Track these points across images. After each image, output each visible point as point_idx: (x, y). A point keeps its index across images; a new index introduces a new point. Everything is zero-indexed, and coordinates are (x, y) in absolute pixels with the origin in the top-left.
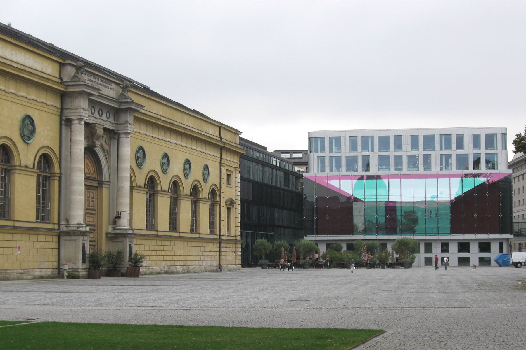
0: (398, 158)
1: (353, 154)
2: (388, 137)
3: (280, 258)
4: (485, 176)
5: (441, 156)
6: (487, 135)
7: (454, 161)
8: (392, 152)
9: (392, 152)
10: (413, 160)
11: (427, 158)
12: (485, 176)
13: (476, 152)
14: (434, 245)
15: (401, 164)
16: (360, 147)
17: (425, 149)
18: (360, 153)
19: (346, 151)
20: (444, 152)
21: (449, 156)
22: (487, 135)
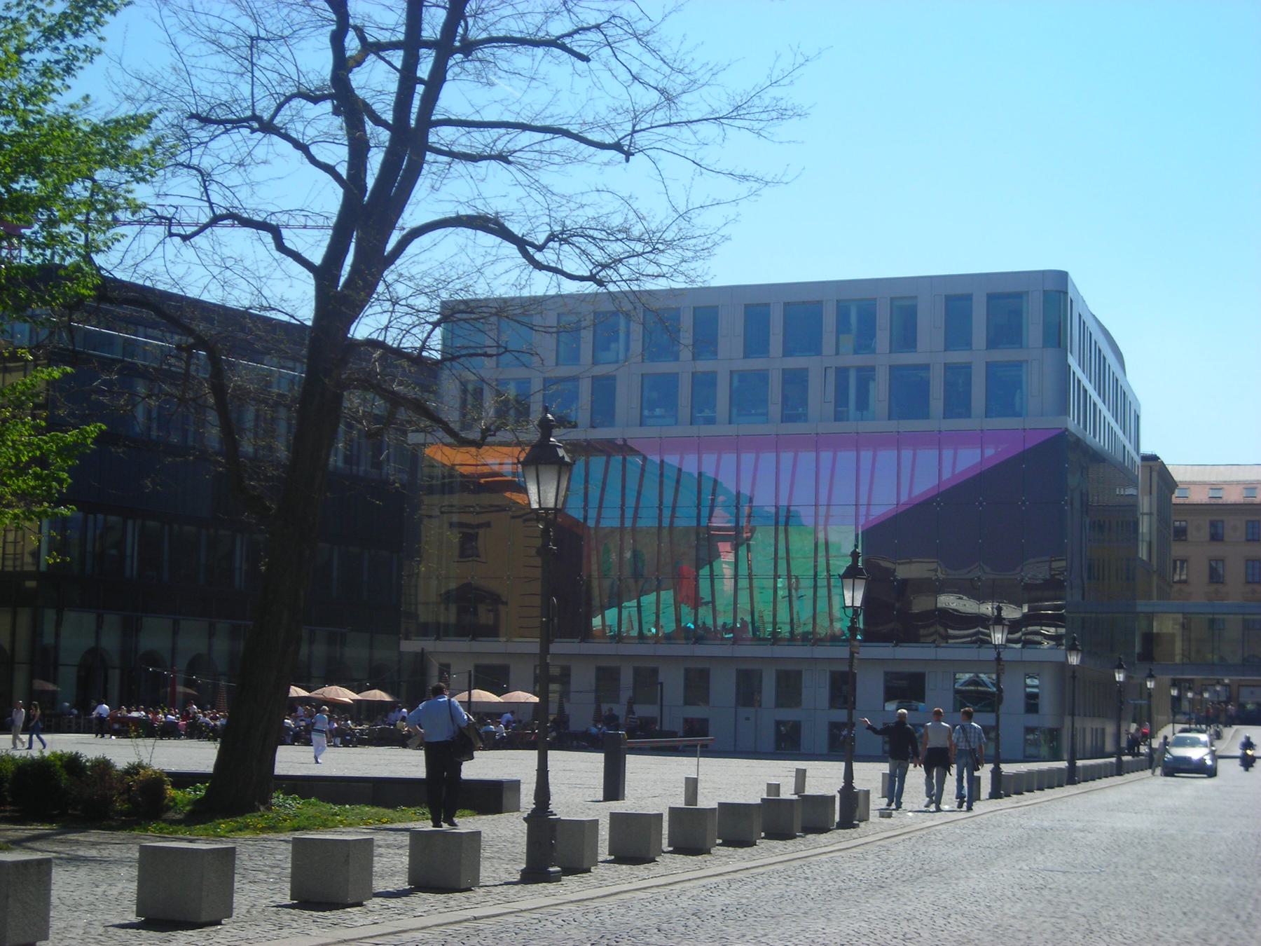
0: (705, 383)
1: (756, 364)
2: (968, 298)
3: (1085, 656)
4: (981, 439)
5: (842, 372)
6: (991, 297)
7: (880, 390)
8: (684, 366)
9: (684, 366)
10: (748, 393)
11: (796, 381)
12: (981, 439)
13: (958, 357)
14: (806, 679)
15: (949, 386)
16: (882, 339)
17: (788, 352)
18: (776, 362)
19: (730, 356)
20: (851, 360)
21: (866, 375)
22: (991, 297)
